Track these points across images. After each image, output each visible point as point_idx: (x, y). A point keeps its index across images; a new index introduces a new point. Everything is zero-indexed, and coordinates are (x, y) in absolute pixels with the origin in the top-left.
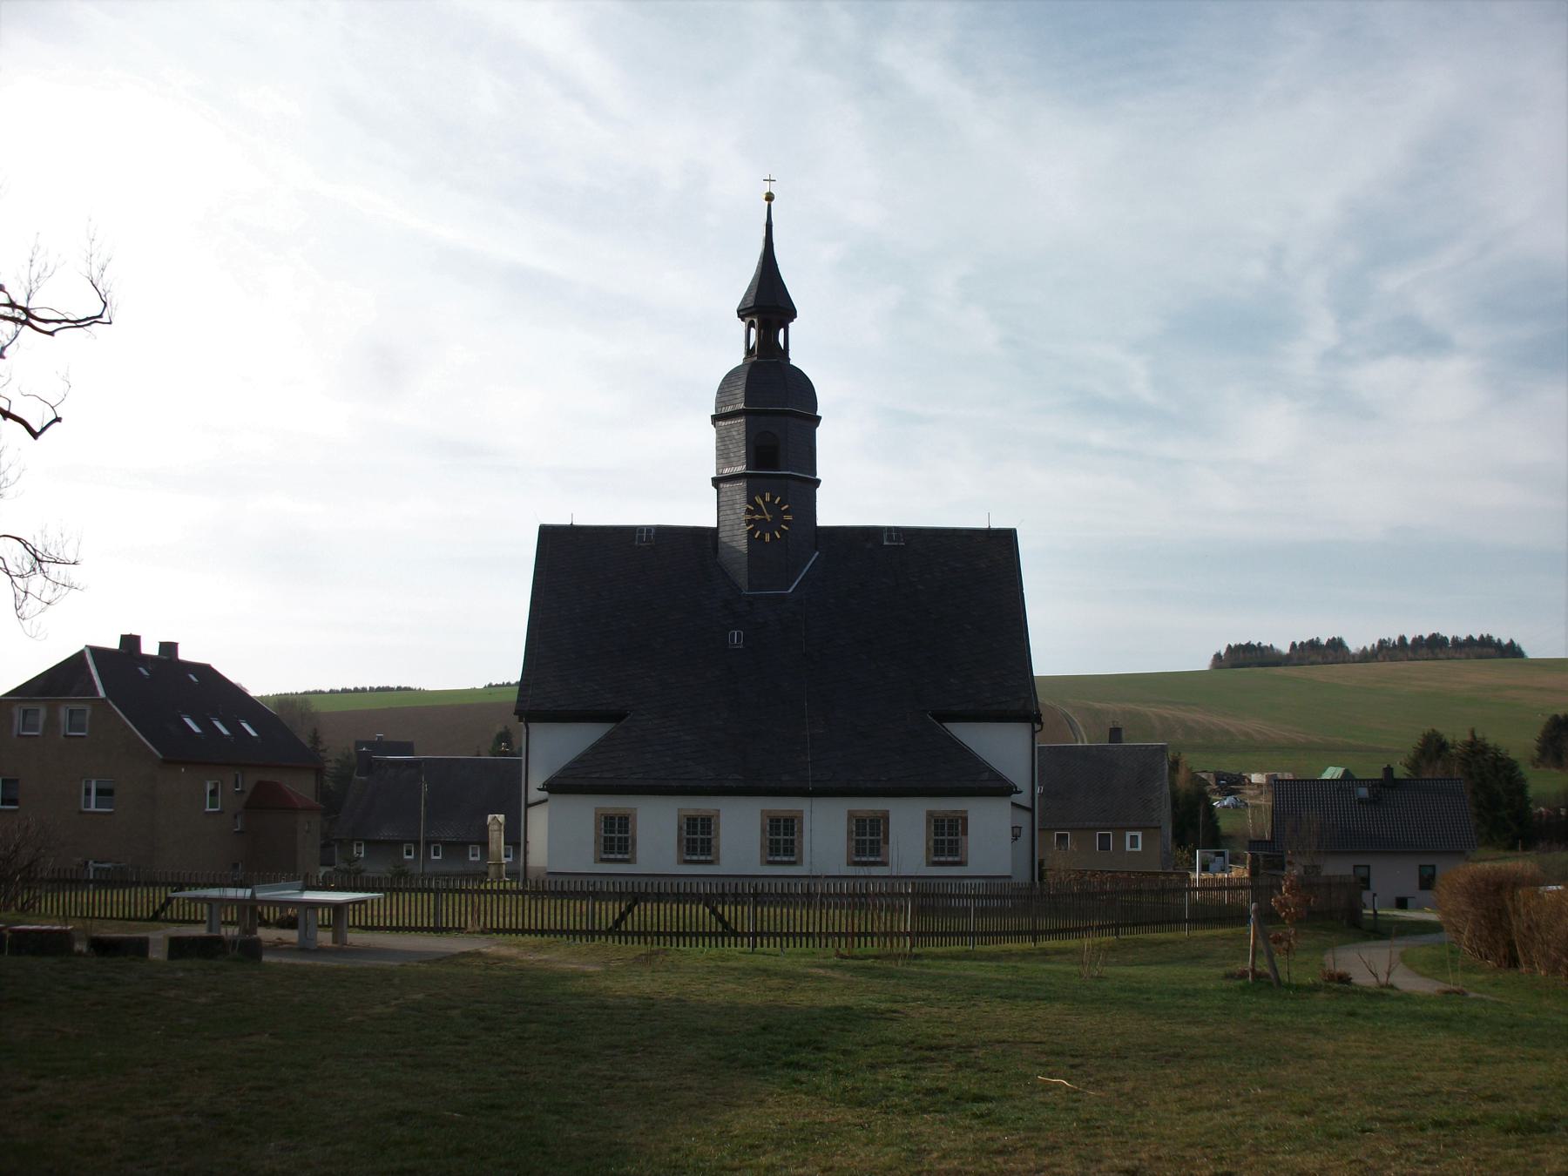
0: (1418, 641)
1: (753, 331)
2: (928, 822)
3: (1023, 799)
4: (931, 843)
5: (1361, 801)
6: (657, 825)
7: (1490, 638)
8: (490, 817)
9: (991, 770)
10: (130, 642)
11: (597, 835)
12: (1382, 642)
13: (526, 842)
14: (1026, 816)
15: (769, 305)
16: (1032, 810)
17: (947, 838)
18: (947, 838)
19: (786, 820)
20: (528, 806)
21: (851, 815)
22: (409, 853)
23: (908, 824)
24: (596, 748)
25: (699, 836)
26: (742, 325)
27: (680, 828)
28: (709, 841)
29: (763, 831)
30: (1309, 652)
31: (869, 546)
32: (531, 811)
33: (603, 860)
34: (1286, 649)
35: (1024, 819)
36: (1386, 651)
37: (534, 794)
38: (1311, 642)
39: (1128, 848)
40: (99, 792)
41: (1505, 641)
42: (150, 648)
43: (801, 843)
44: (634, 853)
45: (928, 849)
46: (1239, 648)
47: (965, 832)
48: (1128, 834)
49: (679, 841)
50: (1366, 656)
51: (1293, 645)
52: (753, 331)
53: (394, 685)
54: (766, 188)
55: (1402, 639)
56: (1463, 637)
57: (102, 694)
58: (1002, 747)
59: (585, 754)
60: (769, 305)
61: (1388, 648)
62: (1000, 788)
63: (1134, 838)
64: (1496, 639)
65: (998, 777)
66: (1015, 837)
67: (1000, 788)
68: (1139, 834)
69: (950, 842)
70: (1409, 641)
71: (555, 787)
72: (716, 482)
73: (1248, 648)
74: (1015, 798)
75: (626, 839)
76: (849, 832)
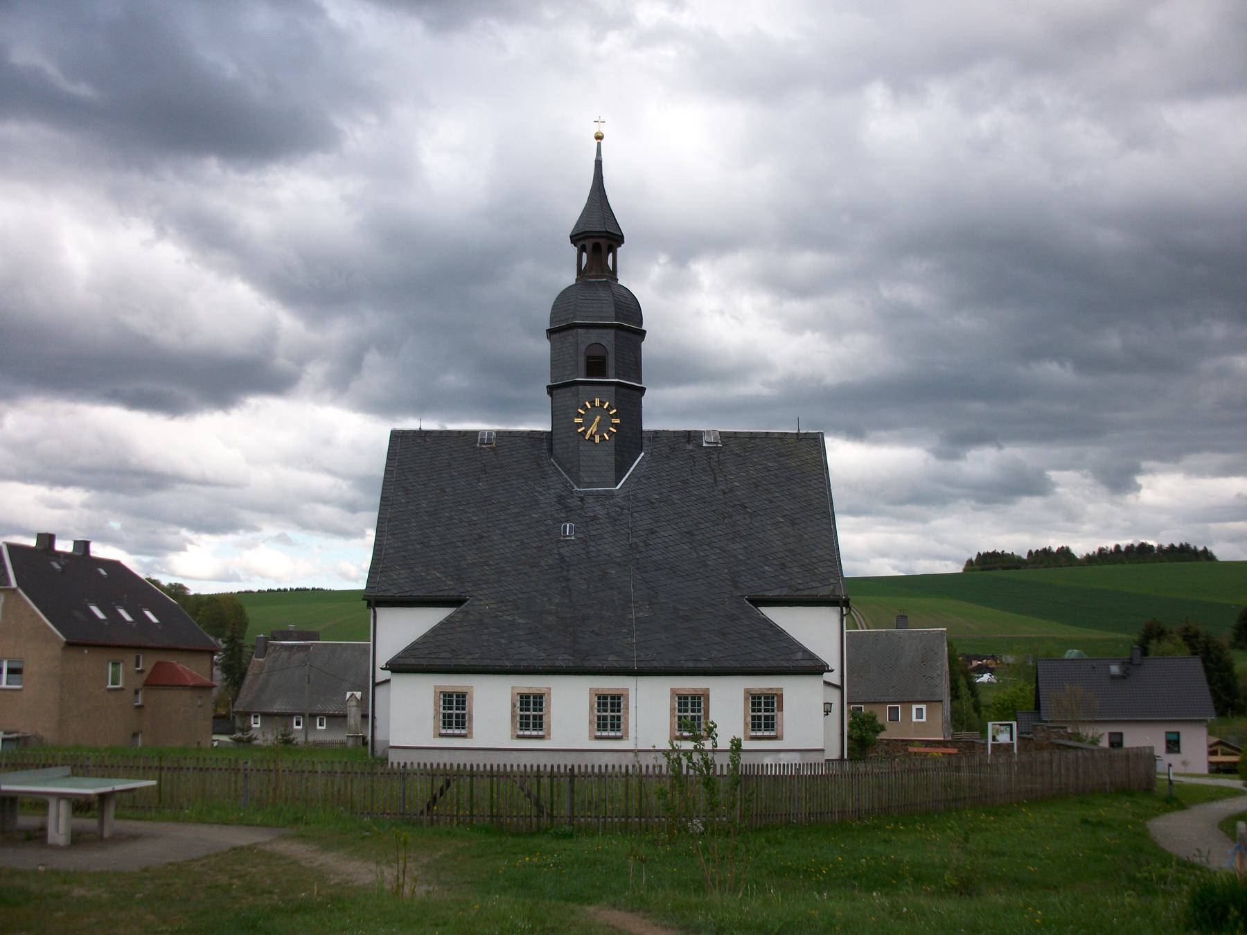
0: (1130, 548)
1: (584, 255)
2: (746, 699)
3: (834, 677)
4: (749, 719)
5: (1113, 677)
6: (492, 701)
7: (1188, 545)
8: (349, 694)
9: (805, 651)
10: (47, 540)
11: (436, 711)
12: (1101, 550)
13: (373, 717)
14: (837, 693)
15: (599, 164)
16: (841, 688)
17: (764, 713)
18: (764, 713)
19: (613, 698)
20: (375, 685)
21: (674, 692)
22: (298, 724)
23: (727, 701)
24: (434, 631)
25: (532, 713)
26: (574, 250)
27: (514, 705)
28: (541, 717)
29: (591, 708)
30: (1043, 558)
31: (690, 447)
32: (379, 690)
33: (441, 735)
34: (1025, 557)
35: (834, 697)
36: (1102, 557)
37: (382, 675)
38: (1044, 550)
39: (914, 719)
40: (10, 671)
41: (1200, 548)
42: (64, 546)
43: (627, 719)
44: (471, 728)
45: (746, 724)
46: (987, 555)
47: (780, 709)
48: (914, 707)
49: (513, 717)
50: (1090, 559)
51: (1030, 552)
52: (584, 255)
53: (309, 586)
54: (595, 129)
55: (1117, 547)
56: (1166, 545)
57: (14, 584)
58: (816, 629)
59: (425, 636)
60: (599, 164)
61: (1106, 554)
62: (815, 668)
63: (919, 711)
64: (1192, 546)
65: (812, 657)
66: (827, 712)
67: (815, 668)
68: (924, 707)
69: (767, 718)
70: (1123, 549)
71: (399, 666)
72: (551, 389)
73: (994, 555)
74: (827, 676)
75: (464, 715)
76: (672, 709)
